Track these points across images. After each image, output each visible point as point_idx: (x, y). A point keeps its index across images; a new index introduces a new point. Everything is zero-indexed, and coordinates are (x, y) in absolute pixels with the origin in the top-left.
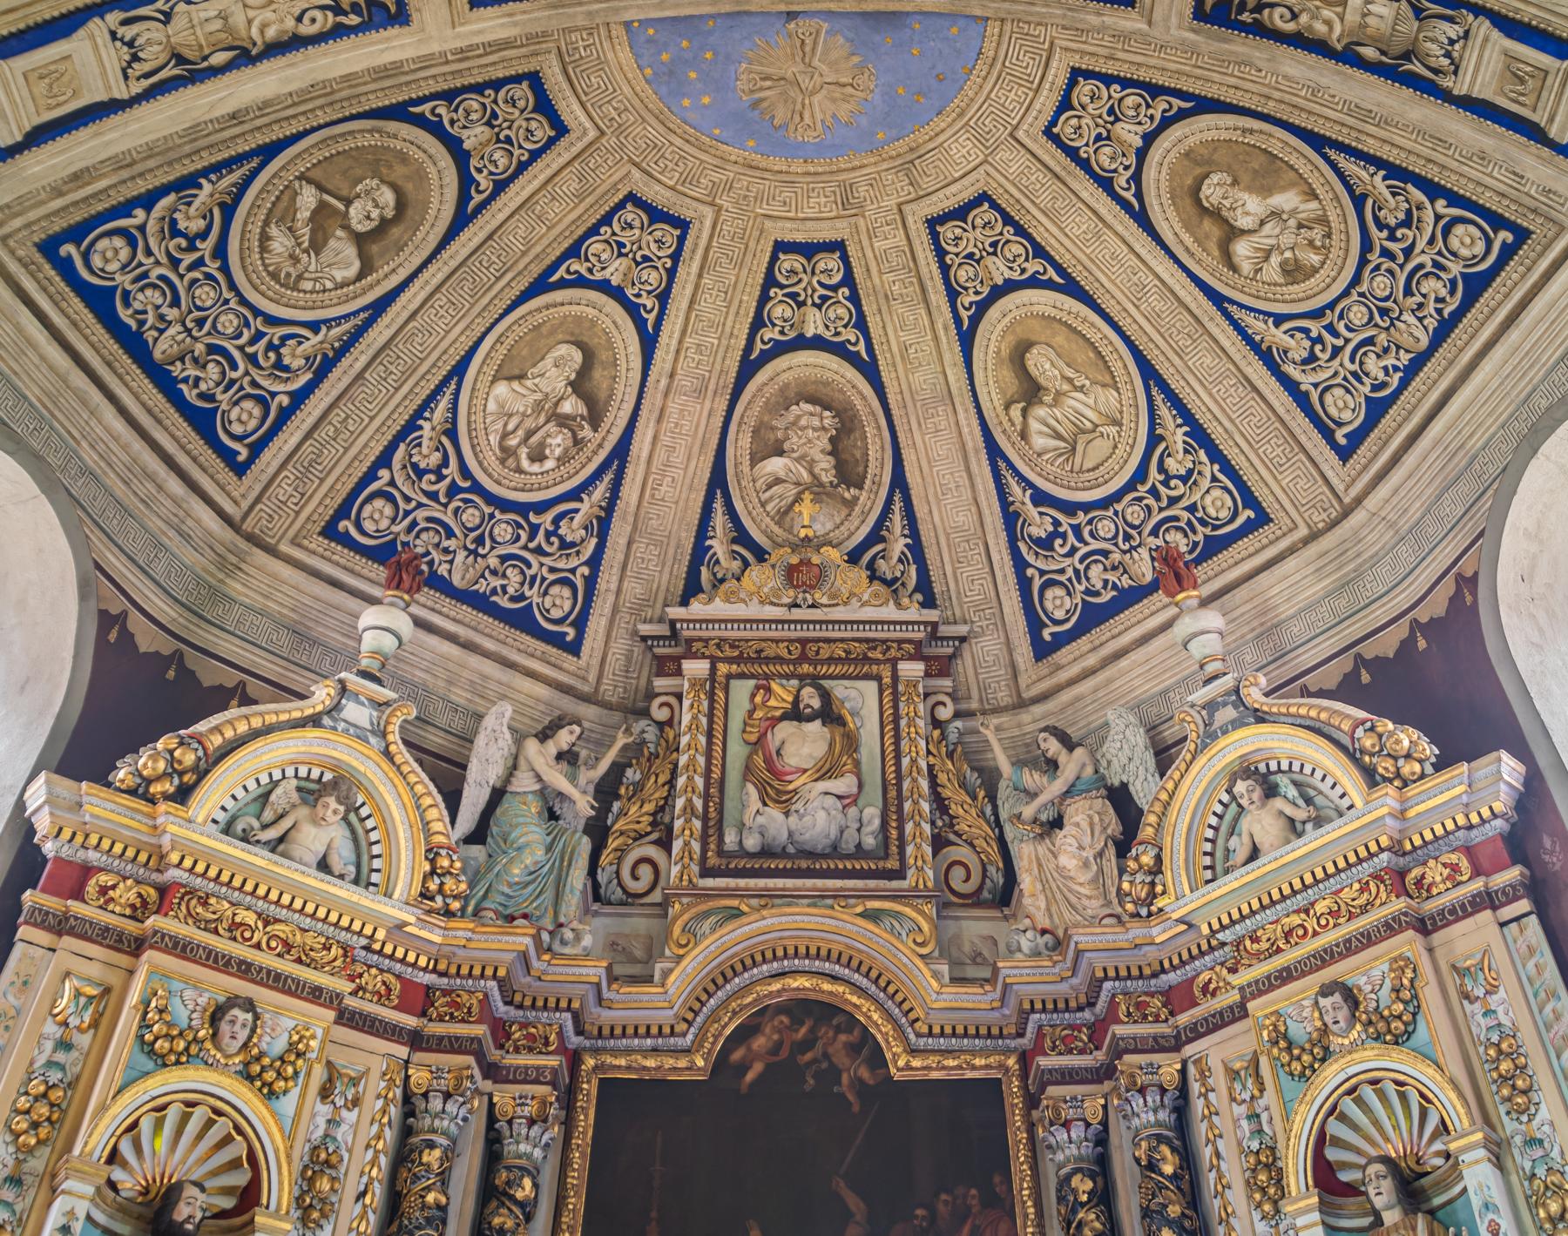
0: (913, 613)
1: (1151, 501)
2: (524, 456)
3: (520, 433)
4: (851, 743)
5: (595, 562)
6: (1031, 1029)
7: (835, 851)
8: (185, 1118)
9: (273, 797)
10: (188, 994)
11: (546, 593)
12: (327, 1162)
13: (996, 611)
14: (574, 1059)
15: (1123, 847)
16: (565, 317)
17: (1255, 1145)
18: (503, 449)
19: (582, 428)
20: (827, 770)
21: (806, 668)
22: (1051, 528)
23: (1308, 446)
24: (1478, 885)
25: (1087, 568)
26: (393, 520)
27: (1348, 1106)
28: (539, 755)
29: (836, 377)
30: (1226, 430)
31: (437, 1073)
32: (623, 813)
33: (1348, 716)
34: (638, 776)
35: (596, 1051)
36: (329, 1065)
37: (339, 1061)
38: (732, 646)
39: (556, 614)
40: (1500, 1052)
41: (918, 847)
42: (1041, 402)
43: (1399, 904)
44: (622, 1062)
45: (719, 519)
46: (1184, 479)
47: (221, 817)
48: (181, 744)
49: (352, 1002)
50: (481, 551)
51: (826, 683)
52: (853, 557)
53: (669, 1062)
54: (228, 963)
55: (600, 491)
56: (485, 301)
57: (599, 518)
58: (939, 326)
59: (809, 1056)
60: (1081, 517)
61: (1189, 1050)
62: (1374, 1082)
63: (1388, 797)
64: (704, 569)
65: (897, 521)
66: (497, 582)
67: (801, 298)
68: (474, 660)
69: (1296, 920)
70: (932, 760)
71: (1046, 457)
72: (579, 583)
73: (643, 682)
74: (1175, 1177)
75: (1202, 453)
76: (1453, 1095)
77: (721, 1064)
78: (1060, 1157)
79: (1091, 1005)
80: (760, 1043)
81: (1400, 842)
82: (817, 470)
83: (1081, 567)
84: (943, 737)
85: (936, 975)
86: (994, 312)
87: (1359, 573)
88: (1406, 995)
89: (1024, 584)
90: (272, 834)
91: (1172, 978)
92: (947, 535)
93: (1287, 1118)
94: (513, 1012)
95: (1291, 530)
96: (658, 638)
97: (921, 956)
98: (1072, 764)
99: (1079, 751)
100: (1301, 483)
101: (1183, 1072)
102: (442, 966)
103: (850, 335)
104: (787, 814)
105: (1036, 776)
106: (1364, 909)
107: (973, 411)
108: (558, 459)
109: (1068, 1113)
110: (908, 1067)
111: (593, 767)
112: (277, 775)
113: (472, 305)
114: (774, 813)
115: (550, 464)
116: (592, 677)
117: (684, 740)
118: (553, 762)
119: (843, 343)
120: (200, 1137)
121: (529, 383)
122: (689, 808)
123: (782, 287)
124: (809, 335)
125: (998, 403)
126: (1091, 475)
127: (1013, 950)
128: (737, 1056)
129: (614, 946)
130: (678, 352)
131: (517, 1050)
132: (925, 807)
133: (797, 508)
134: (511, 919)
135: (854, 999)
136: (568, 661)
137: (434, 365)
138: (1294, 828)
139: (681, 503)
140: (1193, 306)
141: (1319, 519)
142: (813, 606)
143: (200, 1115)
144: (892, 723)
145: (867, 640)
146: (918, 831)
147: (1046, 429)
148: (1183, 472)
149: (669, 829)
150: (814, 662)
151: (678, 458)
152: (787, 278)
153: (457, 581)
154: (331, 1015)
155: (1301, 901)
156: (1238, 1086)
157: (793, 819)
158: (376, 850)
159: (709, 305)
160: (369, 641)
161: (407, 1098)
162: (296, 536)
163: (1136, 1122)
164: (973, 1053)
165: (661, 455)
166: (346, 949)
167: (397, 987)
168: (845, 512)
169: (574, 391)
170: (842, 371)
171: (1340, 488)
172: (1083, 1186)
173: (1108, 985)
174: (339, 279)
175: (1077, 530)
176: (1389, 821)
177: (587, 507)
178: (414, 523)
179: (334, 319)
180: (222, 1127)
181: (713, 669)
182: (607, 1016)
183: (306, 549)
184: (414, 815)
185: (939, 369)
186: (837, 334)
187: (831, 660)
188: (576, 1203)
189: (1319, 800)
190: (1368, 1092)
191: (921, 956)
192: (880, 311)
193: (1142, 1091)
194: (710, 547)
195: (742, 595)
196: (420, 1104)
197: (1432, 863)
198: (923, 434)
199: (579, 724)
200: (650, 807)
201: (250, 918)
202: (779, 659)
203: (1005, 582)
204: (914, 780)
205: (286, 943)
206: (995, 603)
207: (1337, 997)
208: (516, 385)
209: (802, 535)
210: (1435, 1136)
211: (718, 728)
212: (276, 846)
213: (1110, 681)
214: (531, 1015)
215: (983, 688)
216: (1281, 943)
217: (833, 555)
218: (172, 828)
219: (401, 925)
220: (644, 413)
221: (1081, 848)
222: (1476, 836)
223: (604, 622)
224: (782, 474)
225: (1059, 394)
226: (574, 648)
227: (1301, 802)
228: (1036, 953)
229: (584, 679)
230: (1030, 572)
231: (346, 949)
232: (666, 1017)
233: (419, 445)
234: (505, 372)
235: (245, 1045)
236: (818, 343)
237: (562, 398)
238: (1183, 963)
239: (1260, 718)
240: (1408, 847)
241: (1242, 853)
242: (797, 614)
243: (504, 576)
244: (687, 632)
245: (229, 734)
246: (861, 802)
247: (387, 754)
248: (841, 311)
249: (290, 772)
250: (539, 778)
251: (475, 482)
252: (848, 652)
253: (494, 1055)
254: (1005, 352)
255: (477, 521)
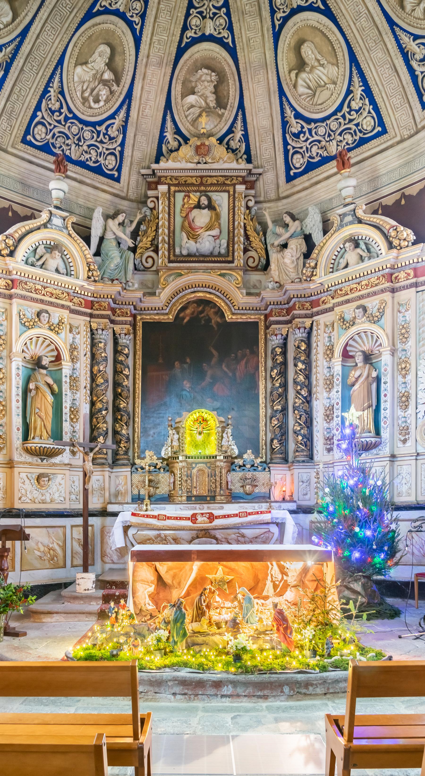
0: (243, 165)
1: (342, 120)
2: (91, 101)
3: (89, 90)
4: (218, 217)
5: (122, 145)
6: (269, 309)
7: (211, 255)
8: (37, 341)
9: (38, 251)
10: (29, 310)
11: (106, 159)
12: (75, 348)
13: (274, 162)
14: (134, 316)
15: (307, 256)
16: (101, 30)
17: (328, 344)
18: (83, 98)
19: (113, 85)
20: (209, 228)
21: (202, 188)
22: (300, 129)
23: (411, 100)
24: (414, 280)
25: (311, 147)
26: (46, 134)
27: (357, 337)
28: (113, 224)
29: (218, 56)
30: (379, 90)
31: (99, 324)
32: (141, 241)
33: (389, 224)
34: (145, 228)
35: (140, 314)
36: (70, 324)
37: (72, 323)
38: (176, 179)
39: (110, 167)
40: (403, 327)
41: (239, 253)
42: (304, 71)
43: (388, 285)
44: (148, 317)
45: (169, 124)
46: (357, 111)
47: (24, 259)
48: (7, 238)
49: (72, 307)
50: (80, 144)
51: (210, 194)
52: (221, 140)
53: (162, 317)
54: (37, 300)
55: (122, 114)
56: (66, 25)
57: (122, 126)
58: (265, 29)
59: (202, 315)
60: (313, 125)
61: (315, 318)
62: (365, 332)
63: (394, 252)
64: (163, 145)
65: (239, 123)
66: (88, 156)
67: (204, 14)
68: (84, 188)
69: (355, 286)
70: (245, 221)
71: (303, 97)
72: (117, 154)
73: (143, 191)
74: (305, 350)
75: (367, 100)
76: (385, 338)
77: (177, 317)
78: (273, 343)
79: (288, 303)
80: (188, 311)
81: (394, 266)
82: (208, 101)
83: (309, 147)
84: (250, 213)
85: (242, 293)
86: (290, 23)
87: (414, 159)
88: (381, 311)
89: (286, 152)
90: (40, 263)
91: (314, 298)
92: (259, 130)
93: (339, 339)
94: (116, 306)
95: (394, 137)
96: (148, 175)
97: (238, 288)
98: (294, 226)
99: (297, 222)
100: (404, 117)
101: (312, 324)
102: (95, 295)
103: (225, 33)
104: (196, 242)
105: (281, 229)
106: (376, 285)
107: (275, 73)
108: (105, 101)
109: (277, 332)
110: (232, 318)
111: (130, 226)
112: (37, 244)
113: (62, 28)
114: (192, 242)
115: (102, 103)
116: (125, 190)
117: (160, 216)
118: (117, 227)
119: (221, 38)
120: (42, 344)
121: (89, 66)
122: (163, 239)
123: (196, 8)
124: (207, 34)
125: (286, 70)
126: (320, 107)
127: (266, 288)
128: (181, 315)
129: (143, 284)
130: (150, 44)
131: (119, 316)
132: (242, 239)
133: (200, 120)
134: (112, 280)
135: (216, 299)
136: (116, 184)
137: (50, 61)
138: (362, 259)
139: (154, 117)
140: (380, 26)
141: (406, 133)
142: (205, 163)
143: (41, 340)
144: (232, 209)
145: (225, 176)
146: (239, 247)
147: (304, 84)
148: (357, 108)
149: (157, 247)
150: (206, 186)
151: (152, 96)
152: (198, 3)
153: (73, 157)
154: (68, 312)
155: (358, 280)
156: (327, 329)
157: (198, 244)
158: (71, 264)
159: (163, 18)
160: (55, 194)
161: (91, 330)
162: (13, 144)
163: (296, 336)
164: (251, 314)
165: (145, 95)
166: (68, 294)
167: (83, 302)
168: (219, 120)
169: (108, 68)
170: (221, 52)
171: (418, 120)
172: (279, 350)
173: (294, 299)
174: (5, 23)
175: (310, 130)
176: (392, 260)
177: (118, 121)
178: (54, 135)
179: (7, 43)
180: (47, 342)
181: (169, 189)
182: (143, 305)
183: (17, 149)
184: (81, 254)
185: (263, 51)
186: (220, 33)
187: (212, 185)
188: (139, 353)
189: (372, 250)
190: (363, 335)
191: (238, 288)
192: (239, 20)
193: (299, 328)
194: (166, 136)
195: (179, 159)
196: (95, 332)
197: (402, 272)
198: (253, 83)
199: (125, 212)
200: (150, 239)
201: (40, 287)
202: (192, 185)
203: (279, 151)
204: (239, 230)
205: (51, 293)
206: (274, 159)
207: (361, 310)
208: (84, 67)
209: (202, 132)
210: (378, 346)
211: (172, 212)
212: (42, 266)
213: (312, 193)
214: (121, 306)
215: (266, 193)
216: (349, 292)
217: (213, 140)
218: (12, 265)
219: (83, 286)
220: (137, 76)
221: (292, 256)
222: (419, 265)
223: (128, 169)
224: (194, 103)
225: (313, 67)
226: (118, 180)
227: (366, 251)
228: (273, 289)
229: (122, 191)
230: (289, 147)
231: (68, 294)
232: (160, 305)
233: (50, 99)
234: (80, 61)
235: (48, 322)
236: (211, 38)
237: (103, 72)
238: (318, 294)
239: (360, 221)
240: (396, 267)
241: (343, 265)
242: (200, 166)
243: (90, 153)
244: (159, 174)
245: (20, 233)
246: (220, 238)
247: (70, 235)
248: (222, 21)
249: (41, 243)
250: (115, 234)
251: (74, 115)
252: (218, 181)
253: (113, 318)
254: (292, 45)
255: (77, 131)
